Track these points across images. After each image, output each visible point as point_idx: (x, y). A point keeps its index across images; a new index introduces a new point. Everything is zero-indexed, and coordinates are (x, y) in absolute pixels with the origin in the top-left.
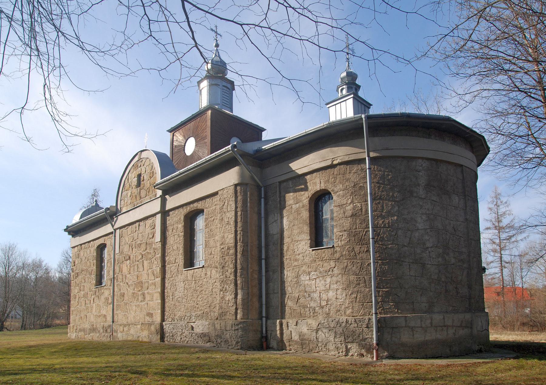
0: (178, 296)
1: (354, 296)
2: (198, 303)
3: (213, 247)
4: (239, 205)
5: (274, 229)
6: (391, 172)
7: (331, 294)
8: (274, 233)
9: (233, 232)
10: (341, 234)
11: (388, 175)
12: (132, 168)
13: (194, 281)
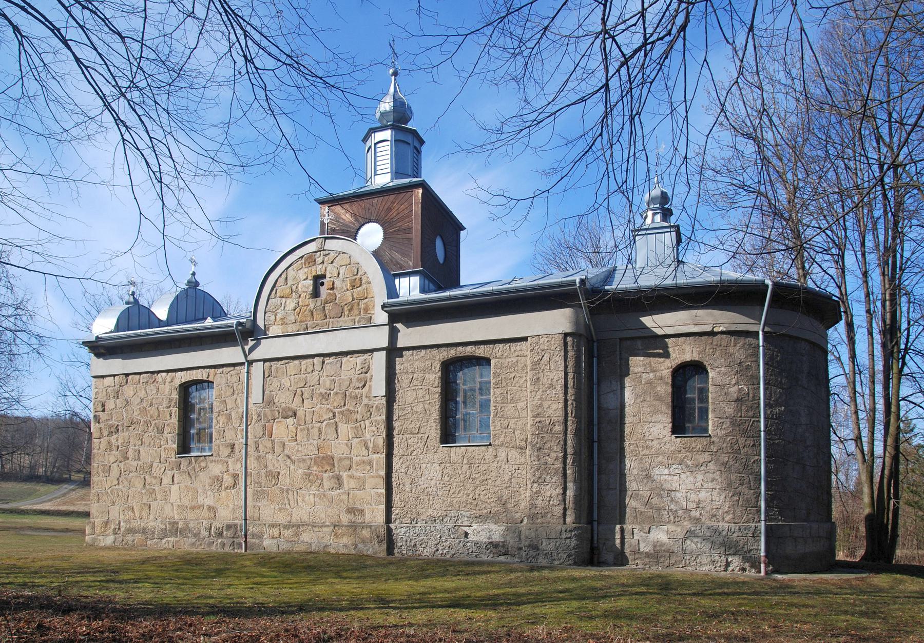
0: (426, 486)
1: (736, 498)
2: (477, 497)
3: (514, 418)
4: (571, 364)
5: (610, 402)
6: (780, 352)
7: (703, 495)
8: (610, 408)
9: (562, 401)
10: (722, 421)
11: (777, 356)
12: (297, 261)
13: (467, 464)
